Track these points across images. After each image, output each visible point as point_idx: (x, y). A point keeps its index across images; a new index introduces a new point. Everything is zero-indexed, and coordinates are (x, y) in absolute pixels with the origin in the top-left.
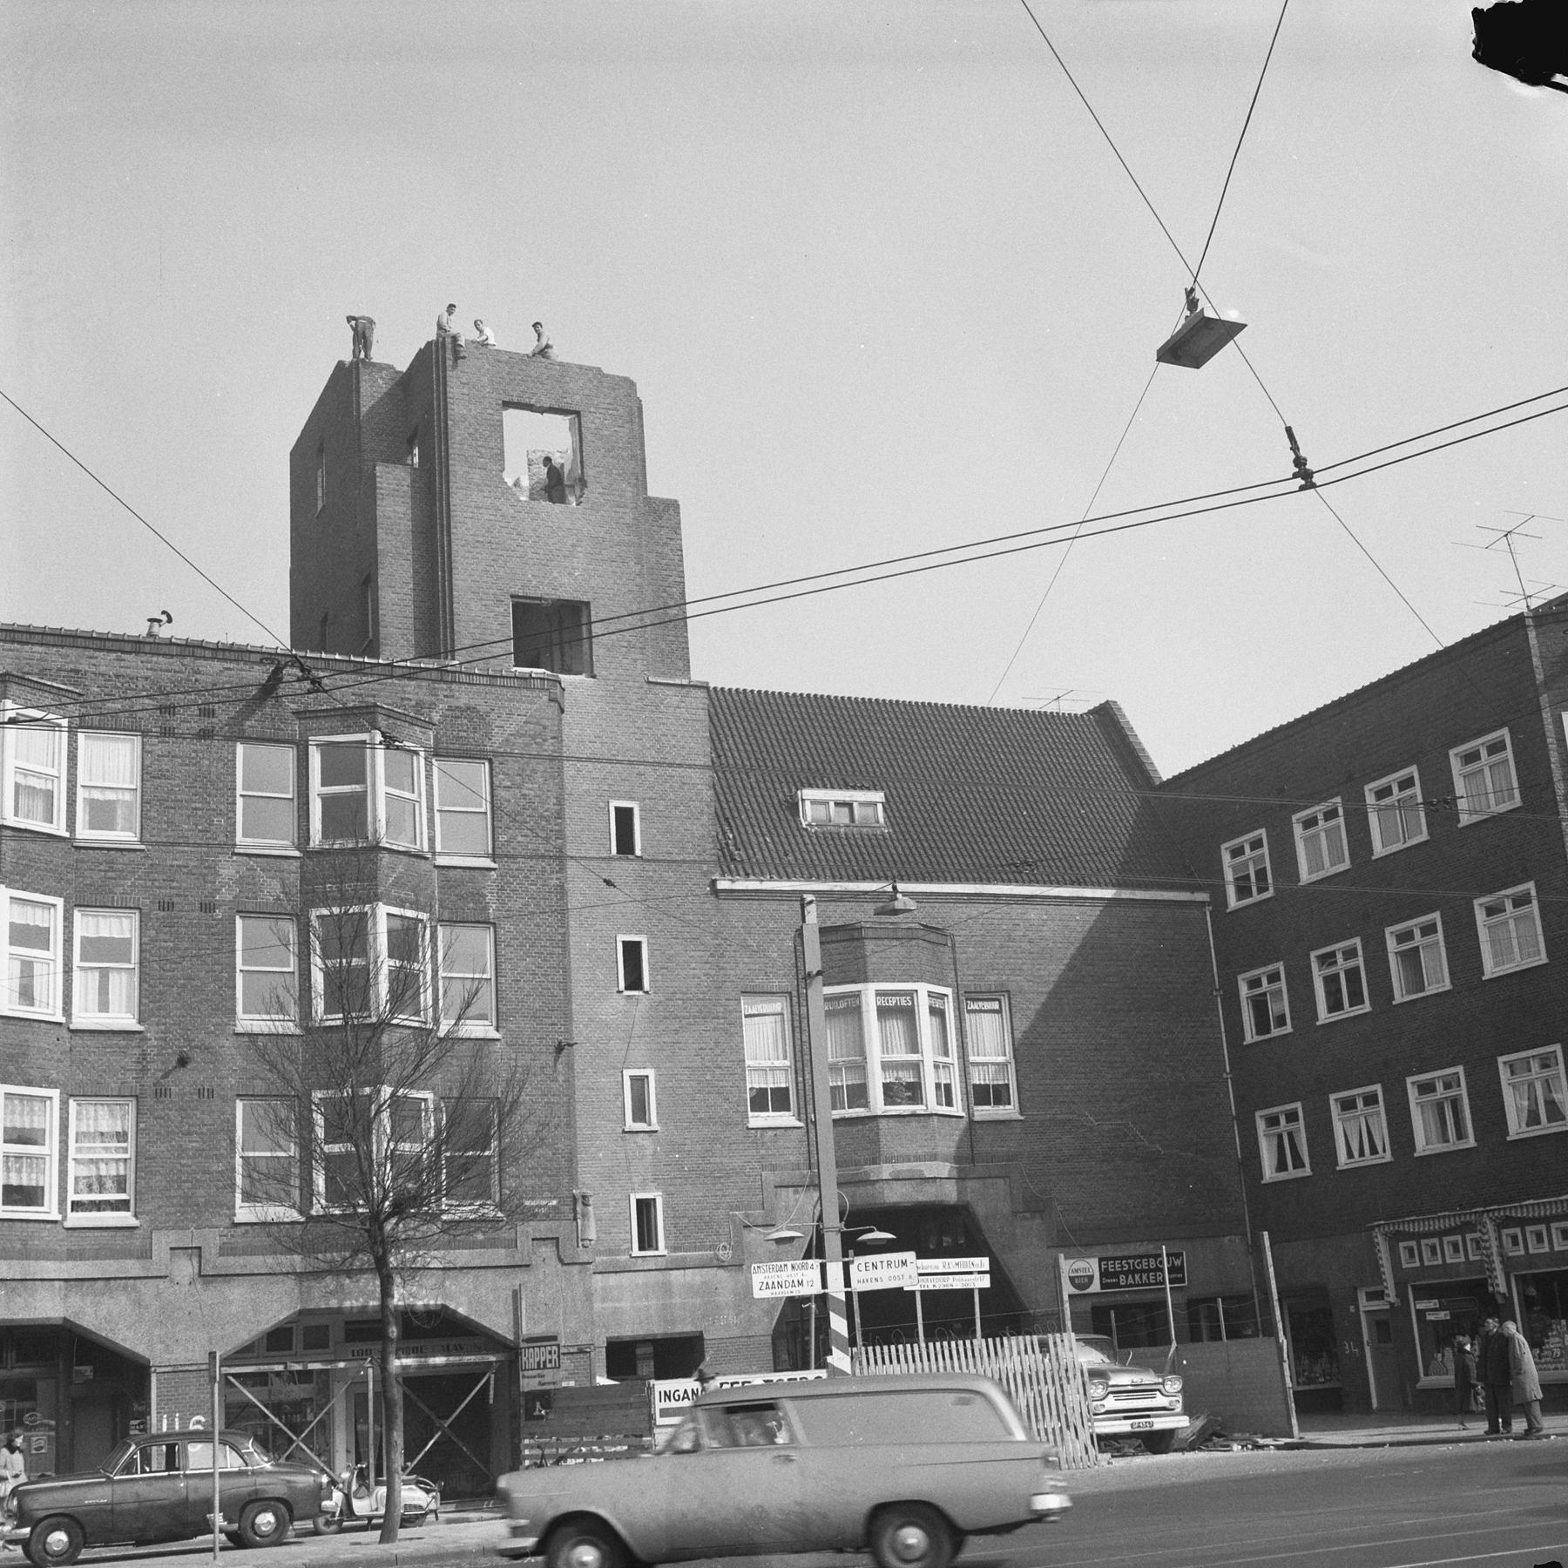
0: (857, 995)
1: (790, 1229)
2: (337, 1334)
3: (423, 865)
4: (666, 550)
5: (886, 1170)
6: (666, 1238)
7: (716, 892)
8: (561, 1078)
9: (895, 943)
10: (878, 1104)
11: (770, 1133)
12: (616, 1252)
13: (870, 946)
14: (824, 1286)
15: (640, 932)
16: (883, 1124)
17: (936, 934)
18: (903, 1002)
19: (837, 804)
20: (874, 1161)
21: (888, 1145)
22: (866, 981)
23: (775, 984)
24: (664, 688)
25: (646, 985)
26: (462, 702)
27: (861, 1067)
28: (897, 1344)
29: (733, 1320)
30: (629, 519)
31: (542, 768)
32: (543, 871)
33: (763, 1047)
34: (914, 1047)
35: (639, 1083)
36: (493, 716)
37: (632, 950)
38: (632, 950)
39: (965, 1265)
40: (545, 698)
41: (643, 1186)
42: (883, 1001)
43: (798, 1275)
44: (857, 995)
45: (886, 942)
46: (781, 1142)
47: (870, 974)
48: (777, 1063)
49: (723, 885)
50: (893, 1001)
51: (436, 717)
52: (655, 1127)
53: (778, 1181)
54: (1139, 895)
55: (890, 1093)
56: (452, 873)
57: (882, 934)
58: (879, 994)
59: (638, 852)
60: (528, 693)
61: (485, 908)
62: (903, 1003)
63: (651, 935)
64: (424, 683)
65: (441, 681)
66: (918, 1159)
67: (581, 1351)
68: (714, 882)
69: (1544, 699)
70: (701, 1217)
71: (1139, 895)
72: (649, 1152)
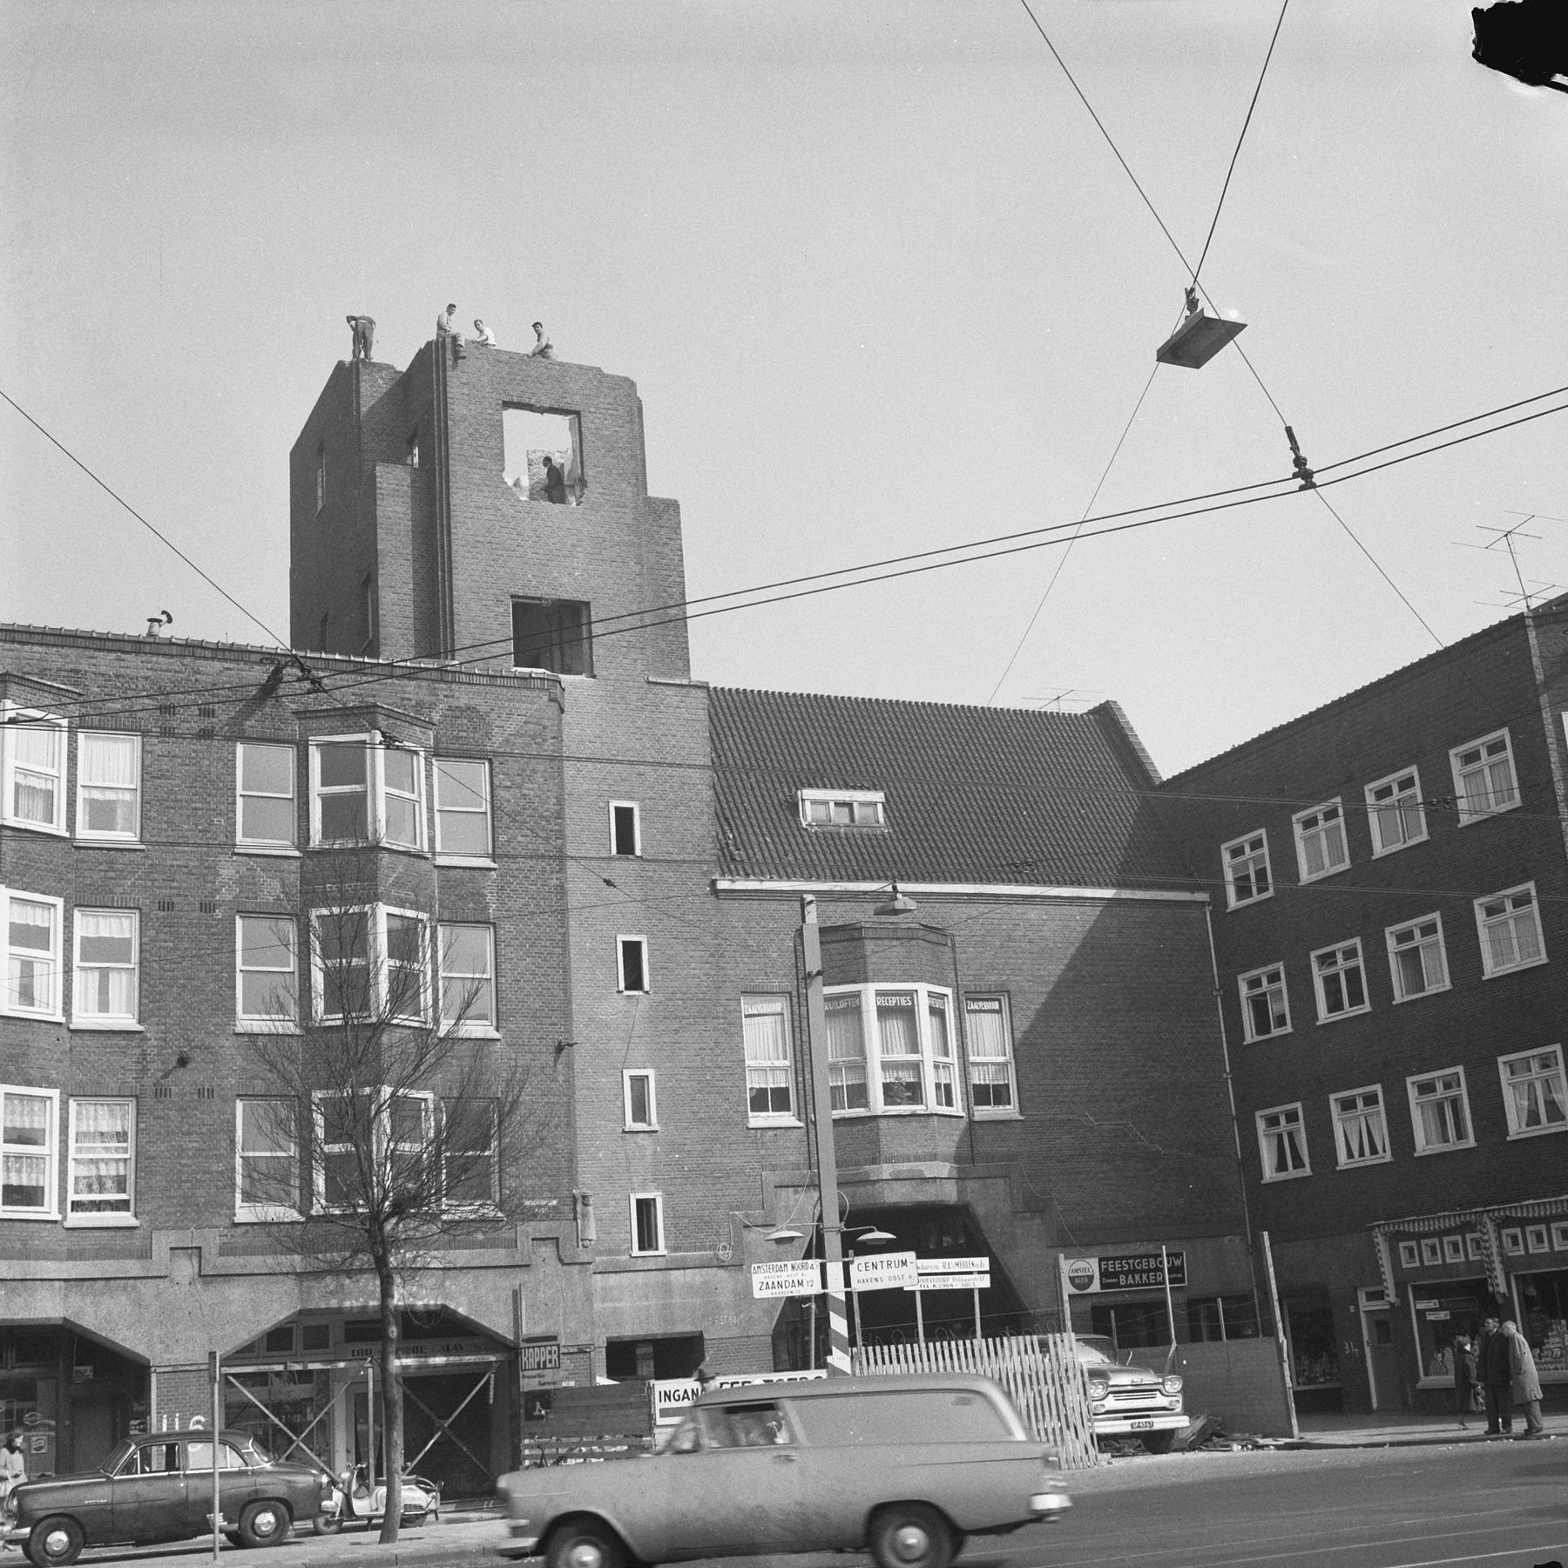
0: (857, 995)
1: (790, 1229)
2: (337, 1334)
3: (423, 865)
4: (666, 550)
5: (886, 1170)
6: (666, 1238)
7: (716, 892)
8: (561, 1078)
9: (895, 943)
10: (878, 1104)
11: (770, 1133)
12: (616, 1252)
13: (870, 946)
14: (824, 1286)
15: (640, 932)
16: (883, 1124)
17: (936, 934)
18: (903, 1002)
19: (837, 804)
20: (874, 1161)
21: (888, 1145)
22: (866, 981)
23: (775, 984)
24: (664, 688)
25: (646, 985)
26: (462, 702)
27: (861, 1067)
28: (897, 1344)
29: (733, 1320)
30: (629, 519)
31: (542, 768)
32: (543, 871)
33: (763, 1047)
34: (914, 1047)
35: (639, 1083)
36: (493, 716)
37: (632, 950)
38: (632, 950)
39: (965, 1265)
40: (545, 698)
41: (643, 1186)
42: (883, 1001)
43: (798, 1275)
44: (857, 995)
45: (886, 942)
46: (781, 1142)
47: (870, 974)
48: (777, 1063)
49: (723, 885)
50: (893, 1001)
51: (436, 717)
52: (655, 1127)
53: (778, 1181)
54: (1139, 895)
55: (890, 1093)
56: (452, 873)
57: (882, 934)
58: (879, 994)
59: (638, 852)
60: (528, 693)
61: (485, 908)
62: (903, 1003)
63: (651, 935)
64: (424, 683)
65: (441, 681)
66: (918, 1159)
67: (581, 1351)
68: (714, 882)
69: (1544, 699)
70: (701, 1217)
71: (1139, 895)
72: (649, 1152)
